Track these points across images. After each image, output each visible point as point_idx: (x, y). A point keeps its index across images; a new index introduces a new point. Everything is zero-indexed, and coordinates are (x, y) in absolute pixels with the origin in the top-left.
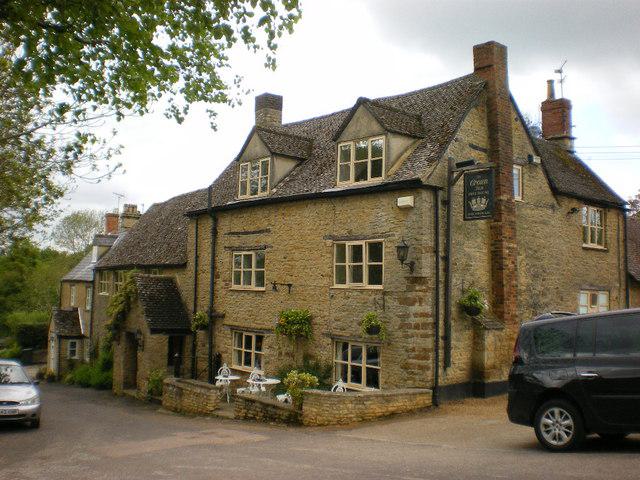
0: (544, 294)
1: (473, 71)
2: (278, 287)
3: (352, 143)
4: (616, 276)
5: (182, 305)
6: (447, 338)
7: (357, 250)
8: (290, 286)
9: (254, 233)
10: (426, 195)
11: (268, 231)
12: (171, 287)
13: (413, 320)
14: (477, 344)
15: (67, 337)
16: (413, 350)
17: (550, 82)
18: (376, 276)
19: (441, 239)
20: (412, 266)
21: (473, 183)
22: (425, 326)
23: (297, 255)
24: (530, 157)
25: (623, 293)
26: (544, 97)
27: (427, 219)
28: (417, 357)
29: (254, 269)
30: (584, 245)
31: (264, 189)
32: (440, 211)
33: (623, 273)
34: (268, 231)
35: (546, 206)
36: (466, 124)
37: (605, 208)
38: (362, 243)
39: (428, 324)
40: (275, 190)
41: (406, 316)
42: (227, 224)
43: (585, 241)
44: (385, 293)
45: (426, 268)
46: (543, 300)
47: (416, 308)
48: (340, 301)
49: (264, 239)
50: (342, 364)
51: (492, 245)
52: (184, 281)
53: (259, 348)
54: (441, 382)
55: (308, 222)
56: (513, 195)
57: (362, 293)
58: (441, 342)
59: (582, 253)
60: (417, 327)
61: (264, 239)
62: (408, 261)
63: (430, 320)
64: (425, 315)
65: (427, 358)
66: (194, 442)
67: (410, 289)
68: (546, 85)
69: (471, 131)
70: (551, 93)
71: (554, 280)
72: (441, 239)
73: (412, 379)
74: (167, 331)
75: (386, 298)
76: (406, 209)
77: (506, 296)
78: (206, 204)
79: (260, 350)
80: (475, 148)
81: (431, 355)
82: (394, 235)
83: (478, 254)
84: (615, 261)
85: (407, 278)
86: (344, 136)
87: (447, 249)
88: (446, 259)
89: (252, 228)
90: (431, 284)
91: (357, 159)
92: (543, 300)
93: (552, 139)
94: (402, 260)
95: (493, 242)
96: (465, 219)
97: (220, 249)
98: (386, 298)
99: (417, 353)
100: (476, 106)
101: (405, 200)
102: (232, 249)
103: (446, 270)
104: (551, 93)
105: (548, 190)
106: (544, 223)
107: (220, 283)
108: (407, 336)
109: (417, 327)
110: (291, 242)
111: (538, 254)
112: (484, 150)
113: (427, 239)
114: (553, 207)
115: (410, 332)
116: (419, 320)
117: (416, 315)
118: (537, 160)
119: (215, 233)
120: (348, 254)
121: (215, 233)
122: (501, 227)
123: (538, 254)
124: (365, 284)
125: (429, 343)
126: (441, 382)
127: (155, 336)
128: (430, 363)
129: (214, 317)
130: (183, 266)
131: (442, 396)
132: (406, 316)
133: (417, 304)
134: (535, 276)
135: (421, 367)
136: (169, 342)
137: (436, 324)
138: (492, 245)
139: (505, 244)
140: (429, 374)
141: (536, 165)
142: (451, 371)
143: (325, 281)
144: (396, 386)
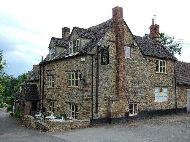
0: (139, 89)
1: (111, 17)
4: (171, 83)
5: (37, 92)
6: (97, 103)
8: (59, 86)
9: (52, 70)
10: (88, 57)
11: (54, 70)
12: (35, 86)
13: (85, 98)
14: (109, 105)
15: (17, 102)
16: (85, 107)
17: (153, 19)
19: (95, 71)
20: (84, 80)
21: (104, 53)
22: (88, 99)
24: (133, 44)
25: (174, 89)
26: (151, 25)
27: (89, 64)
28: (86, 110)
29: (52, 81)
30: (157, 72)
31: (54, 57)
32: (94, 63)
33: (174, 82)
34: (54, 70)
35: (141, 60)
36: (107, 34)
37: (166, 60)
39: (89, 99)
40: (56, 57)
41: (83, 96)
43: (157, 70)
45: (89, 81)
46: (138, 91)
47: (86, 94)
48: (69, 92)
49: (54, 72)
52: (38, 85)
53: (53, 106)
54: (94, 118)
55: (61, 67)
56: (124, 56)
58: (94, 105)
59: (156, 75)
60: (86, 100)
61: (54, 72)
62: (83, 78)
63: (90, 97)
64: (88, 96)
65: (89, 110)
67: (84, 87)
68: (151, 20)
69: (109, 35)
70: (153, 23)
71: (143, 84)
72: (95, 71)
73: (84, 117)
74: (30, 101)
75: (79, 90)
76: (83, 62)
77: (120, 90)
78: (69, 62)
80: (110, 41)
81: (91, 109)
83: (111, 76)
84: (170, 77)
85: (83, 84)
86: (70, 40)
87: (97, 74)
88: (97, 78)
89: (51, 69)
90: (91, 86)
91: (73, 46)
92: (138, 91)
93: (152, 38)
96: (102, 65)
97: (45, 75)
98: (79, 90)
100: (111, 28)
101: (83, 59)
102: (48, 75)
103: (97, 81)
104: (153, 23)
105: (141, 54)
106: (140, 65)
108: (83, 103)
109: (86, 100)
111: (137, 76)
112: (114, 42)
113: (89, 71)
114: (143, 60)
115: (84, 101)
116: (87, 98)
117: (86, 96)
118: (136, 45)
122: (118, 67)
123: (137, 76)
124: (75, 86)
125: (90, 105)
126: (94, 118)
127: (27, 102)
128: (90, 111)
129: (44, 96)
130: (38, 81)
131: (94, 123)
132: (83, 96)
133: (86, 92)
134: (135, 83)
135: (87, 113)
137: (92, 99)
139: (120, 72)
140: (90, 115)
141: (136, 46)
142: (99, 114)
143: (66, 85)
144: (81, 119)
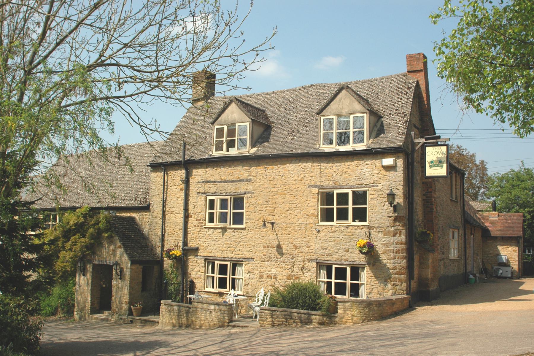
2: (267, 224)
3: (334, 117)
7: (224, 203)
8: (272, 224)
11: (250, 181)
18: (360, 215)
23: (280, 199)
34: (250, 181)
38: (228, 197)
42: (198, 174)
44: (370, 228)
50: (327, 282)
51: (424, 195)
57: (348, 228)
66: (472, 244)
79: (234, 275)
82: (377, 186)
94: (391, 203)
95: (425, 193)
99: (398, 270)
107: (192, 222)
110: (273, 190)
119: (187, 182)
120: (217, 205)
121: (187, 182)
130: (146, 208)
136: (143, 272)
138: (424, 195)
